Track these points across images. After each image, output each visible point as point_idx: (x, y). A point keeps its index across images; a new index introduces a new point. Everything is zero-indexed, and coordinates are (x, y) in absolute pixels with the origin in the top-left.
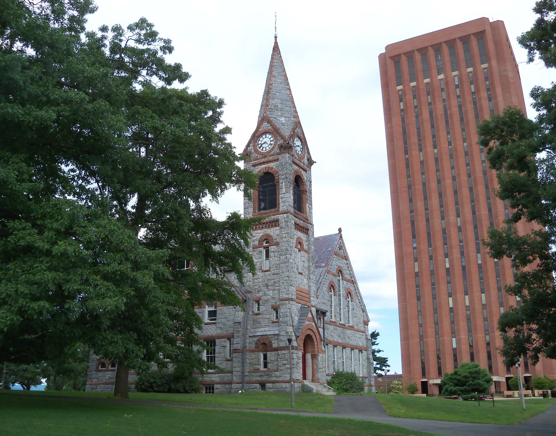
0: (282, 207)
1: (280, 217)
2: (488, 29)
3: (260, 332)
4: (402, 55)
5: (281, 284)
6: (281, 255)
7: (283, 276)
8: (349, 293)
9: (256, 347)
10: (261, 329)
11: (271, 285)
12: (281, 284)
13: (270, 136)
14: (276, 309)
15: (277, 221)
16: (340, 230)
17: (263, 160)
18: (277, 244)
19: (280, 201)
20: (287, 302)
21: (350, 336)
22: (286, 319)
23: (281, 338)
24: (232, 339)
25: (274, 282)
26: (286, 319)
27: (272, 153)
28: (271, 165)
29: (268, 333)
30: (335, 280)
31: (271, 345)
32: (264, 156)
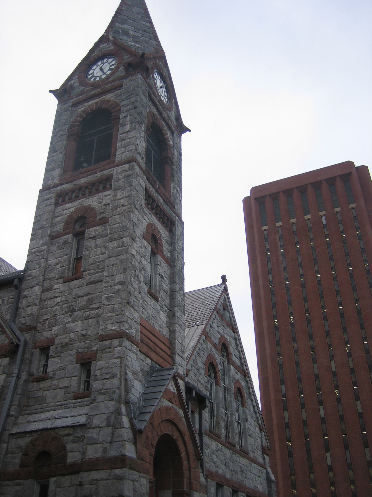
0: (121, 153)
1: (115, 171)
3: (39, 422)
5: (105, 302)
6: (111, 240)
8: (239, 390)
9: (23, 465)
11: (81, 309)
12: (105, 302)
14: (86, 363)
15: (108, 179)
16: (224, 278)
18: (104, 221)
19: (119, 144)
20: (116, 342)
21: (244, 468)
22: (109, 384)
23: (92, 434)
25: (90, 301)
26: (109, 384)
27: (110, 80)
28: (108, 96)
29: (58, 423)
30: (218, 358)
31: (65, 457)
32: (95, 85)
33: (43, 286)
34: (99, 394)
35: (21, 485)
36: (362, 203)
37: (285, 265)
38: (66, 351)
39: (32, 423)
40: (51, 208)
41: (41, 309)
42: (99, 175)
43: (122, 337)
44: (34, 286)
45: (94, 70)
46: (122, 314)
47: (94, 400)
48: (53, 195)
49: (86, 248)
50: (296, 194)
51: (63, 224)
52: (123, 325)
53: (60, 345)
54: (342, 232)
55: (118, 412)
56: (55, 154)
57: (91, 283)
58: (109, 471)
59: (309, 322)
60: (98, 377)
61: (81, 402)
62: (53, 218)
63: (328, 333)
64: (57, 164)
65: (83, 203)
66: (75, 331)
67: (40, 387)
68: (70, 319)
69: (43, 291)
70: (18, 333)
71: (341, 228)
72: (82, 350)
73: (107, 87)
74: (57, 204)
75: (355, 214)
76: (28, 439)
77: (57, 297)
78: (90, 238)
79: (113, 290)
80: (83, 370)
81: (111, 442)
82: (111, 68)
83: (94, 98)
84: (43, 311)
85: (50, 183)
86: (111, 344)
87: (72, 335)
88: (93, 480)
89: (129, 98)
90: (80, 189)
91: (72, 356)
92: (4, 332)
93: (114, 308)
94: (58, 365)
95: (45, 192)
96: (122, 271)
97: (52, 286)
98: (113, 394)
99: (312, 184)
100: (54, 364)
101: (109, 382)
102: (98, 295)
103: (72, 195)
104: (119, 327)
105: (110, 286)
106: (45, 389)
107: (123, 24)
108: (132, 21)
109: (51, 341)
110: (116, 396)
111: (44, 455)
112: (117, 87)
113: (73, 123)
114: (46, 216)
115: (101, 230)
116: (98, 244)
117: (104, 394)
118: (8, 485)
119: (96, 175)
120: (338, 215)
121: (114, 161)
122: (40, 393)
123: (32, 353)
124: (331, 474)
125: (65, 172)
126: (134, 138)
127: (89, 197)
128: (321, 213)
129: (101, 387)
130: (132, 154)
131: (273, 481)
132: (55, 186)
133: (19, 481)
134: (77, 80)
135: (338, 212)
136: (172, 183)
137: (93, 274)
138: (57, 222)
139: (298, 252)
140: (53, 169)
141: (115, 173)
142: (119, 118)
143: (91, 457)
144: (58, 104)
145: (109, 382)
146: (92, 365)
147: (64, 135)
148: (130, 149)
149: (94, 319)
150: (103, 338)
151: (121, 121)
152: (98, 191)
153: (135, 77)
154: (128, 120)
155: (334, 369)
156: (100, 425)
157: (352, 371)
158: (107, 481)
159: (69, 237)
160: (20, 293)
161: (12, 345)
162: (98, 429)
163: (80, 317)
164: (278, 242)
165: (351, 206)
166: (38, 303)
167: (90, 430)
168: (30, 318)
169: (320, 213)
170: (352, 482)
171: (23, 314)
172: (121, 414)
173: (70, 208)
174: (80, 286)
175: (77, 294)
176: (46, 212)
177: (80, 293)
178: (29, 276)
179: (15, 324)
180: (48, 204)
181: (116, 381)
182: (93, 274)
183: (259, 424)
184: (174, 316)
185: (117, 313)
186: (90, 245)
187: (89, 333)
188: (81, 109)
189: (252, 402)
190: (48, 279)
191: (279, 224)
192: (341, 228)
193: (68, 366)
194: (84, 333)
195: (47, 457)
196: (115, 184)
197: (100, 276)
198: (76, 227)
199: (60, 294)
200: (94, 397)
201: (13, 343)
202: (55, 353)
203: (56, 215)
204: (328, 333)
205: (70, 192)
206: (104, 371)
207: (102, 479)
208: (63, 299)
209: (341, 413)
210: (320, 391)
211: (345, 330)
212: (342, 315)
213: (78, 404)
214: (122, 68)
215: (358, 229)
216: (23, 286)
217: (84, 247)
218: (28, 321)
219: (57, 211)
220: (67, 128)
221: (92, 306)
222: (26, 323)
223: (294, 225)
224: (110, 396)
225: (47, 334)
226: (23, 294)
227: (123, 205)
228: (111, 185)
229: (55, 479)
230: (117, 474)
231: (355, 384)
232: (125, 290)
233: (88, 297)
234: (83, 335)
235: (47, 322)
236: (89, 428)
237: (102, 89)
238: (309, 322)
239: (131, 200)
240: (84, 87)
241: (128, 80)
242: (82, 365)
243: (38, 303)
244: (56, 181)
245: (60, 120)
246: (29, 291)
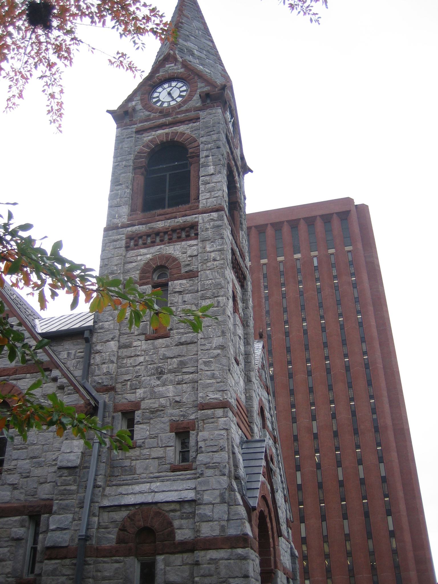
0: (205, 199)
1: (200, 218)
2: (354, 209)
3: (136, 494)
4: (253, 228)
5: (203, 367)
6: (204, 298)
7: (208, 346)
9: (119, 541)
10: (137, 488)
11: (170, 372)
12: (203, 367)
13: (180, 85)
14: (183, 432)
15: (194, 226)
17: (162, 120)
18: (192, 275)
19: (202, 188)
20: (219, 412)
22: (217, 457)
23: (206, 510)
24: (44, 517)
25: (182, 364)
26: (217, 457)
28: (181, 128)
29: (160, 497)
31: (172, 534)
32: (164, 112)
33: (119, 341)
34: (207, 468)
35: (121, 562)
36: (360, 246)
37: (267, 309)
38: (156, 417)
39: (126, 496)
40: (122, 251)
41: (119, 367)
42: (181, 220)
43: (226, 408)
44: (108, 341)
45: (160, 93)
46: (224, 381)
47: (202, 474)
48: (124, 237)
49: (171, 304)
50: (286, 229)
51: (138, 272)
52: (227, 394)
53: (147, 411)
54: (335, 277)
55: (231, 489)
56: (119, 187)
57: (182, 344)
58: (229, 550)
59: (291, 376)
60: (203, 449)
61: (182, 475)
62: (125, 263)
63: (311, 390)
64: (123, 200)
65: (162, 251)
66: (165, 396)
67: (127, 455)
68: (158, 382)
69: (120, 347)
70: (94, 393)
71: (335, 273)
72: (176, 418)
73: (179, 116)
74: (128, 248)
75: (350, 259)
76: (124, 514)
77: (138, 356)
78: (175, 292)
79: (212, 355)
80: (177, 440)
81: (228, 520)
82: (181, 94)
83: (164, 128)
84: (123, 370)
85: (116, 221)
86: (214, 414)
87: (163, 401)
88: (211, 559)
89: (208, 134)
90: (157, 234)
91: (164, 423)
92: (77, 391)
93: (214, 374)
94: (148, 433)
95: (110, 232)
96: (219, 334)
97: (131, 343)
98: (224, 468)
99: (306, 219)
100: (141, 432)
101: (216, 456)
102: (192, 358)
103: (147, 240)
104: (223, 396)
105: (207, 350)
106: (133, 458)
107: (186, 41)
108: (194, 38)
109: (137, 406)
110: (226, 471)
111: (146, 533)
112: (191, 120)
113: (138, 153)
114: (116, 260)
115: (188, 285)
116: (186, 300)
117: (213, 468)
118: (105, 562)
119: (176, 220)
120: (332, 257)
121: (198, 206)
122: (127, 463)
123: (113, 418)
124: (304, 548)
125: (133, 210)
126: (220, 183)
127: (168, 245)
128: (313, 254)
129: (208, 460)
130: (219, 202)
131: (297, 557)
132: (124, 226)
133: (118, 558)
134: (140, 102)
135: (332, 254)
136: (241, 232)
137: (183, 333)
138: (131, 269)
139: (284, 296)
140: (118, 206)
141: (201, 221)
142: (198, 156)
143: (207, 535)
144: (117, 128)
145: (216, 455)
146: (191, 435)
147: (130, 166)
148: (217, 195)
149: (188, 385)
150: (203, 406)
151: (202, 160)
152: (179, 239)
153: (214, 111)
154: (211, 160)
155: (315, 431)
156: (214, 502)
157: (336, 434)
158: (229, 561)
159: (148, 289)
160: (91, 348)
161: (89, 407)
162: (211, 506)
163: (171, 381)
164: (262, 281)
165: (348, 248)
166: (115, 361)
167: (202, 506)
168: (107, 377)
169: (312, 253)
170: (327, 556)
171: (97, 372)
172: (234, 490)
173: (146, 255)
174: (167, 346)
175: (164, 354)
176: (116, 255)
177: (169, 354)
178: (101, 329)
179: (88, 382)
180: (117, 246)
181: (225, 455)
182: (183, 333)
183: (285, 495)
184: (251, 381)
185: (219, 380)
186: (176, 301)
187: (184, 400)
188: (148, 137)
189: (280, 471)
190: (124, 334)
191: (264, 261)
192: (335, 273)
193: (160, 435)
194: (178, 399)
195: (148, 533)
196: (202, 234)
197: (193, 337)
198: (154, 277)
199: (143, 352)
200: (202, 471)
201: (90, 404)
202: (143, 419)
203: (128, 260)
204: (311, 390)
205: (144, 235)
206: (209, 443)
207: (222, 559)
208: (147, 358)
209: (320, 480)
210: (298, 454)
211: (330, 388)
212: (328, 371)
213: (178, 477)
214: (196, 97)
215: (353, 275)
216: (94, 340)
217: (169, 302)
218: (106, 381)
219: (128, 256)
220: (132, 158)
221: (184, 370)
222: (103, 382)
223: (281, 264)
224: (220, 471)
225: (131, 397)
226: (95, 348)
227: (215, 260)
228: (197, 234)
229: (162, 557)
230: (240, 554)
231: (337, 449)
232: (225, 356)
233: (179, 359)
234: (176, 402)
235: (129, 383)
236: (200, 504)
237: (174, 118)
238: (291, 376)
239: (223, 254)
240: (150, 112)
241: (205, 113)
242: (178, 434)
243: (115, 361)
244: (125, 220)
245: (122, 148)
246: (102, 345)
